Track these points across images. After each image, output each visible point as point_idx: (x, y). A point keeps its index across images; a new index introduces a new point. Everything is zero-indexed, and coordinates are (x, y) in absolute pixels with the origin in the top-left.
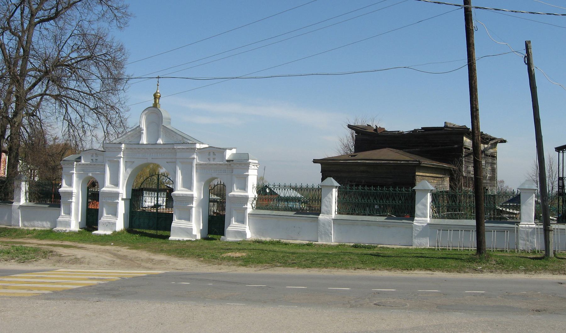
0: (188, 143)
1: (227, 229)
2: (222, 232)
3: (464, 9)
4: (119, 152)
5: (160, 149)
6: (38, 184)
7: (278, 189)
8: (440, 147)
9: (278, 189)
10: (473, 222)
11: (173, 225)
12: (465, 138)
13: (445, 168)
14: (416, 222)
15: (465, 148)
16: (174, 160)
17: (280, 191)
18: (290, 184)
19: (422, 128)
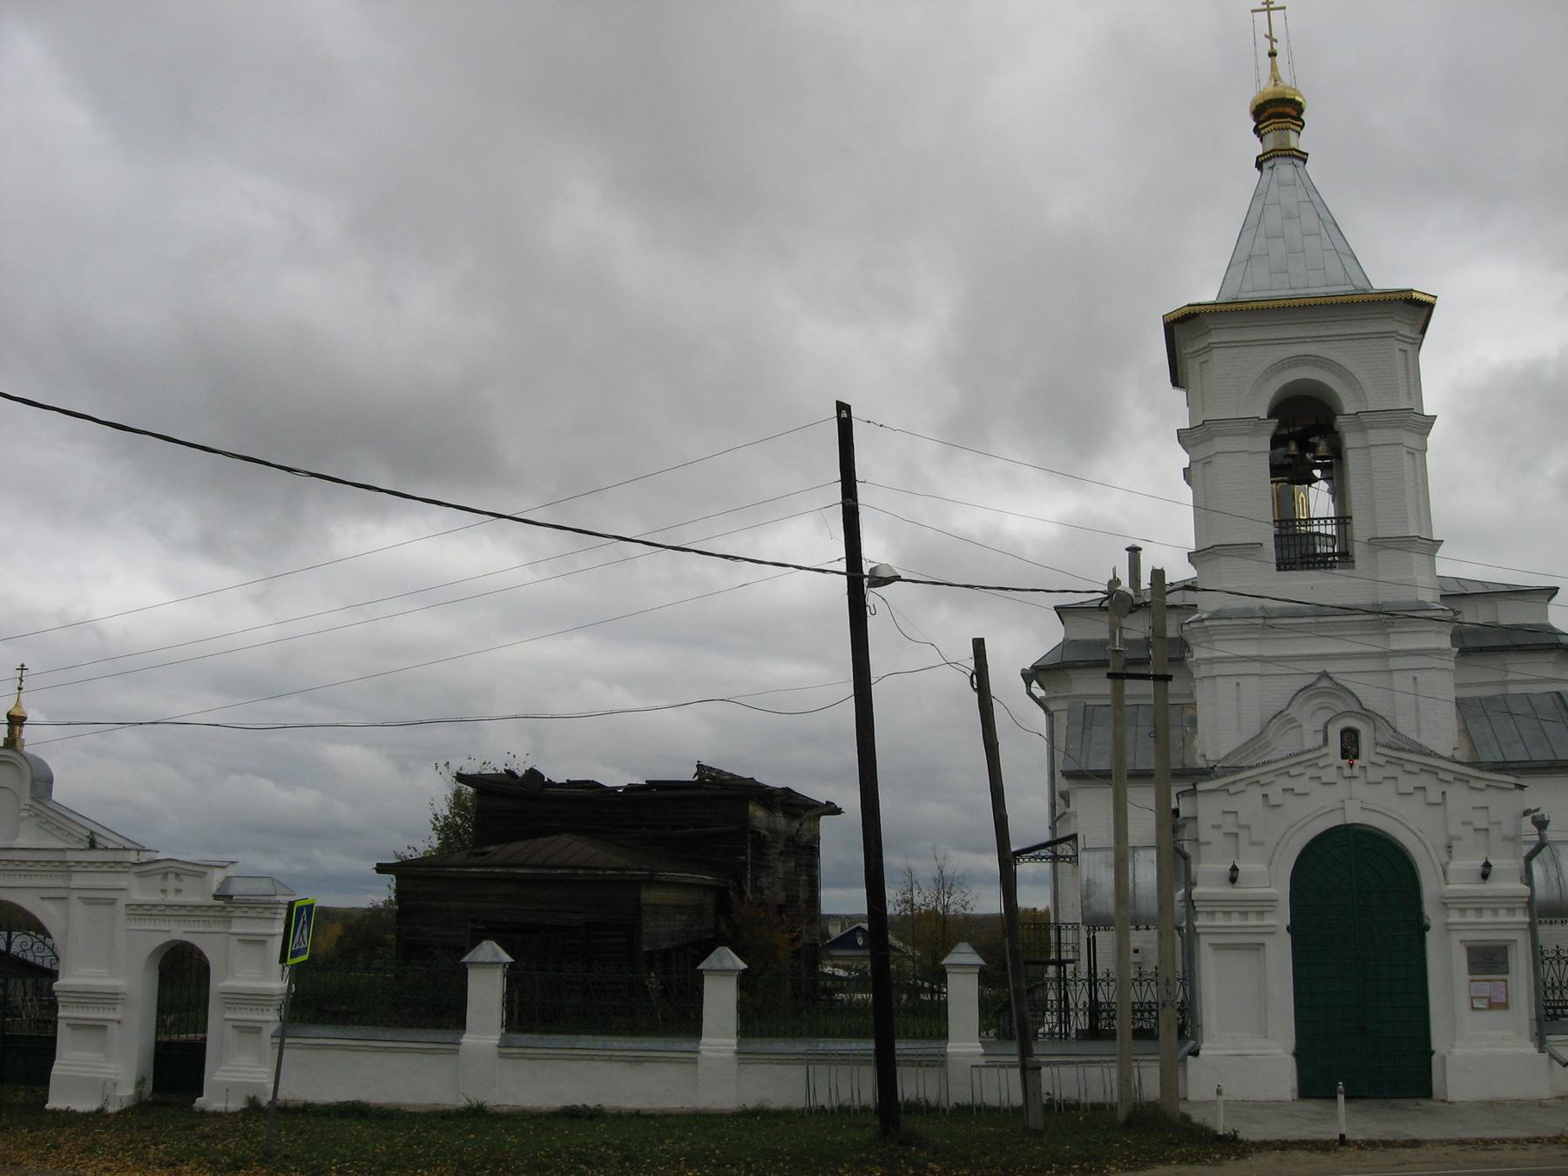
0: (107, 848)
1: (214, 1078)
2: (196, 1086)
3: (845, 564)
4: (945, 921)
5: (21, 861)
6: (830, 992)
7: (1105, 983)
8: (691, 830)
9: (1105, 983)
10: (869, 1045)
11: (58, 1069)
12: (751, 808)
13: (708, 883)
14: (709, 1051)
15: (752, 832)
16: (61, 893)
17: (1144, 989)
18: (1154, 970)
19: (568, 780)
